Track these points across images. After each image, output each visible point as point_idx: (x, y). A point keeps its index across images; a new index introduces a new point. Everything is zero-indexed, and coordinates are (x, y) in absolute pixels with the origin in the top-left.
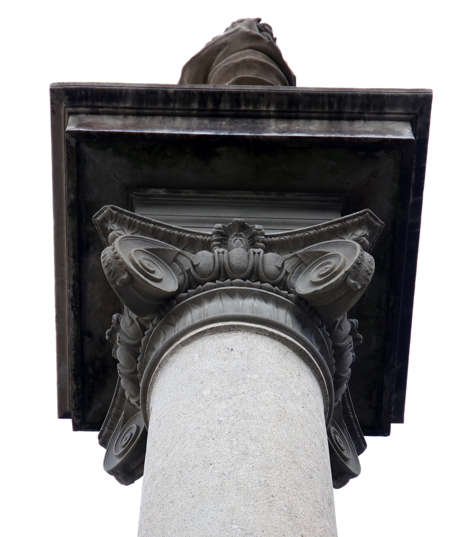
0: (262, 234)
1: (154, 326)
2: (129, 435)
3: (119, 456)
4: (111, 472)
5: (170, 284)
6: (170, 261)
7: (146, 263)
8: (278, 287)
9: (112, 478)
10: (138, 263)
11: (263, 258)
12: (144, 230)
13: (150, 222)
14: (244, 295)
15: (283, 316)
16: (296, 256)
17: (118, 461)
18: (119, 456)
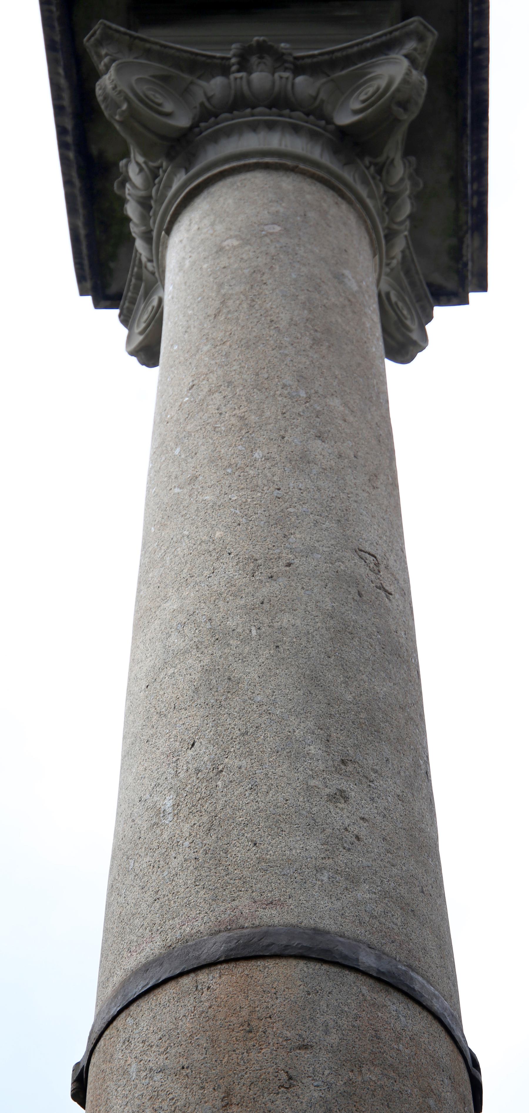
0: (290, 54)
1: (165, 172)
2: (150, 308)
3: (141, 333)
4: (132, 353)
5: (183, 121)
6: (184, 93)
7: (150, 93)
8: (311, 118)
9: (134, 359)
10: (141, 94)
11: (293, 85)
12: (148, 53)
13: (156, 43)
14: (271, 126)
15: (317, 152)
16: (332, 80)
17: (141, 338)
18: (141, 333)
